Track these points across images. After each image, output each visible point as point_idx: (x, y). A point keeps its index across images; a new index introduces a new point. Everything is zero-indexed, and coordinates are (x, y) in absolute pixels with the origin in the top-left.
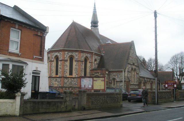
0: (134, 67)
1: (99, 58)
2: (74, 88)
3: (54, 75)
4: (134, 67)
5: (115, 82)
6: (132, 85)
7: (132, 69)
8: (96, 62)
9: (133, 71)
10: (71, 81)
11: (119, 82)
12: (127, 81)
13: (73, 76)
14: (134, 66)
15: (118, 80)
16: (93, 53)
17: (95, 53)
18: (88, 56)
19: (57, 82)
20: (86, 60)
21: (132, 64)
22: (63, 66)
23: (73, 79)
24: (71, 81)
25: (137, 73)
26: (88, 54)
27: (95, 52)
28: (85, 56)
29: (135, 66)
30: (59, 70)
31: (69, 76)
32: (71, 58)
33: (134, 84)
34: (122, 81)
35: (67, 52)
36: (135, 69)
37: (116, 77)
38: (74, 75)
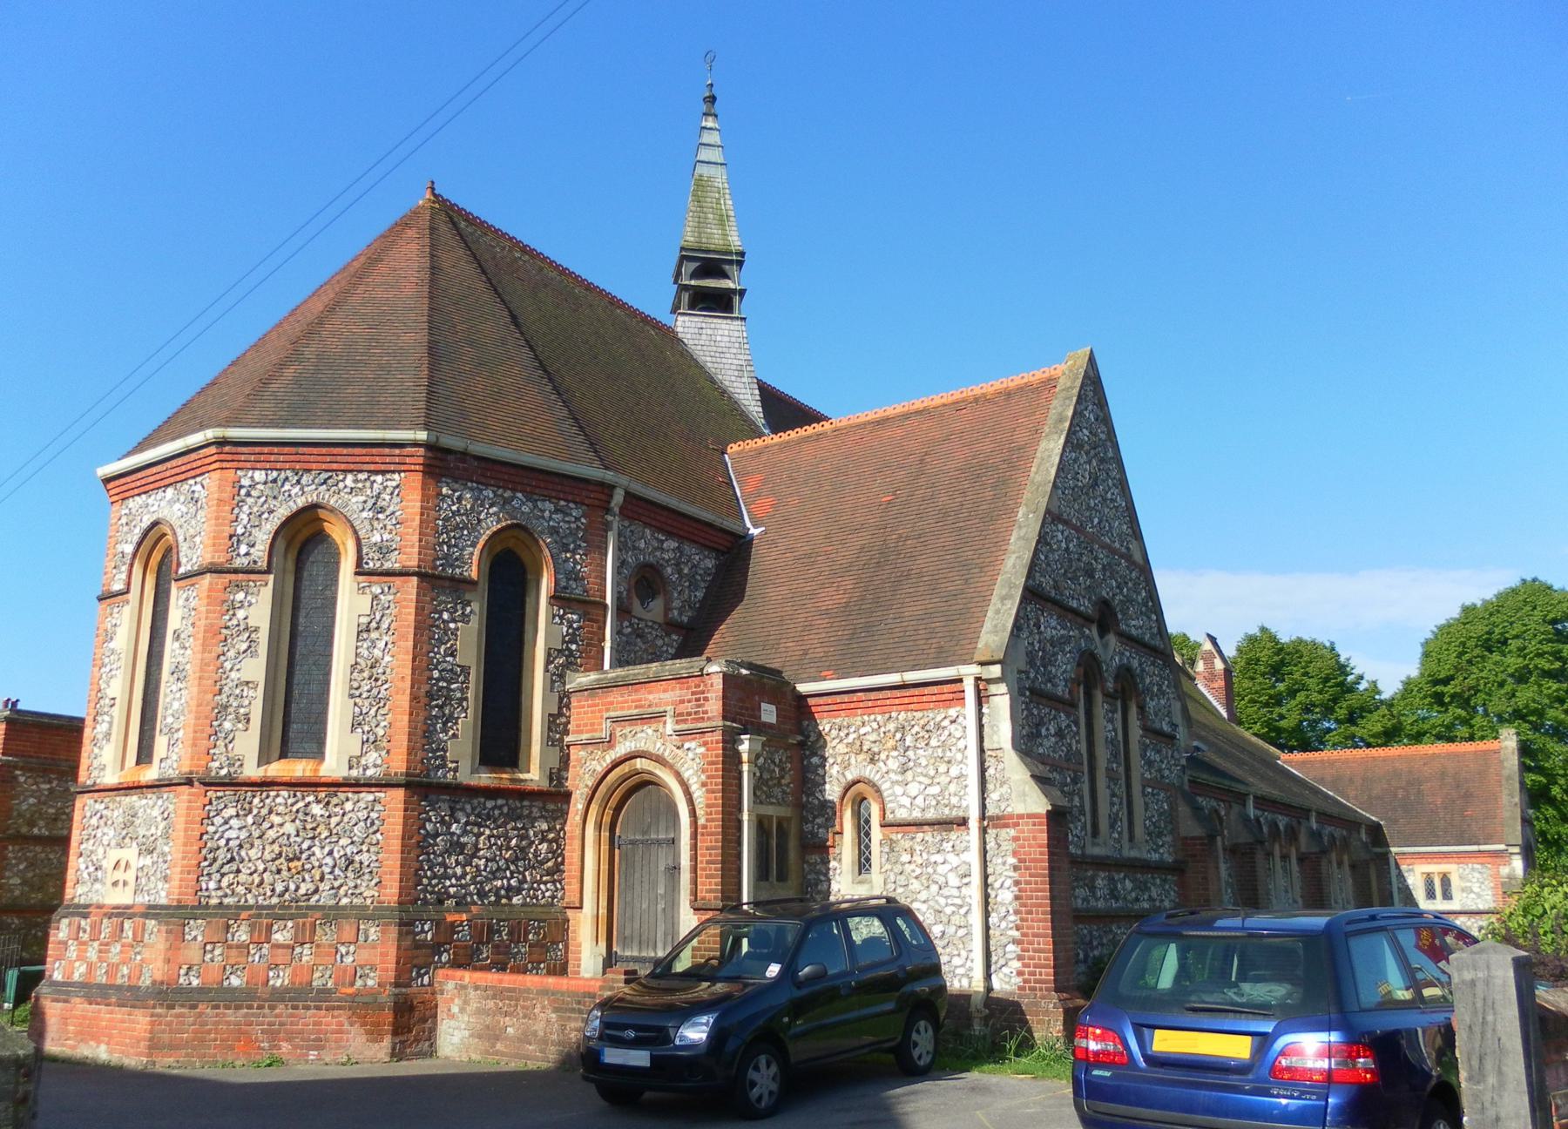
0: (243, 492)
1: (709, 563)
2: (334, 914)
3: (460, 757)
4: (243, 492)
5: (876, 833)
6: (1100, 863)
7: (1089, 668)
8: (657, 605)
9: (1106, 695)
10: (290, 828)
11: (919, 824)
12: (1019, 808)
13: (333, 766)
14: (1112, 639)
15: (904, 798)
16: (607, 489)
17: (628, 494)
18: (538, 526)
19: (130, 853)
20: (304, 539)
21: (1085, 606)
22: (218, 636)
23: (317, 809)
24: (290, 828)
25: (1159, 733)
26: (549, 506)
27: (637, 488)
28: (491, 524)
29: (1126, 638)
30: (175, 700)
31: (485, 779)
32: (304, 539)
33: (1129, 853)
34: (963, 822)
35: (259, 476)
36: (1126, 676)
37: (885, 773)
38: (170, 756)
